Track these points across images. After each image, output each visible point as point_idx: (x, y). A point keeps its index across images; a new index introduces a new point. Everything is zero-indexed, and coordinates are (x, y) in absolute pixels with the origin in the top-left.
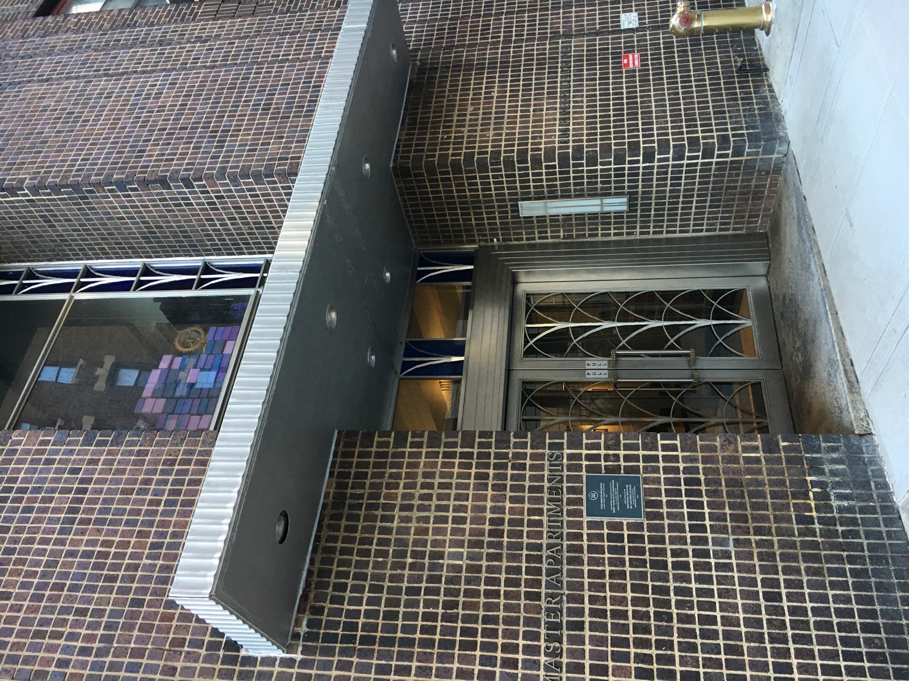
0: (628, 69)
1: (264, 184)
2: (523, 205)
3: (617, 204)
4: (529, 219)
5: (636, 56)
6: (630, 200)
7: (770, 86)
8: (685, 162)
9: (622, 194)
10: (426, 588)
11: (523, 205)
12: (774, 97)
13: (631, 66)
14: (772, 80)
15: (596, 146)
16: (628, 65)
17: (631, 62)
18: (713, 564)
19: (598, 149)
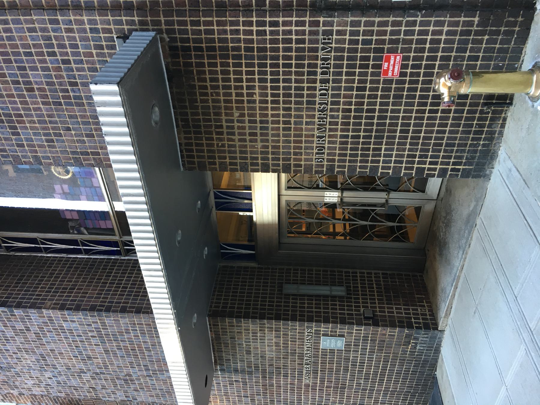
0: (387, 77)
1: (54, 157)
2: (343, 294)
3: (290, 289)
4: (340, 284)
5: (398, 57)
6: (281, 291)
7: (505, 119)
8: (438, 167)
9: (286, 295)
10: (400, 113)
11: (343, 294)
12: (501, 133)
13: (390, 74)
14: (509, 114)
15: (344, 167)
16: (386, 72)
17: (391, 68)
18: (243, 47)
19: (346, 170)
